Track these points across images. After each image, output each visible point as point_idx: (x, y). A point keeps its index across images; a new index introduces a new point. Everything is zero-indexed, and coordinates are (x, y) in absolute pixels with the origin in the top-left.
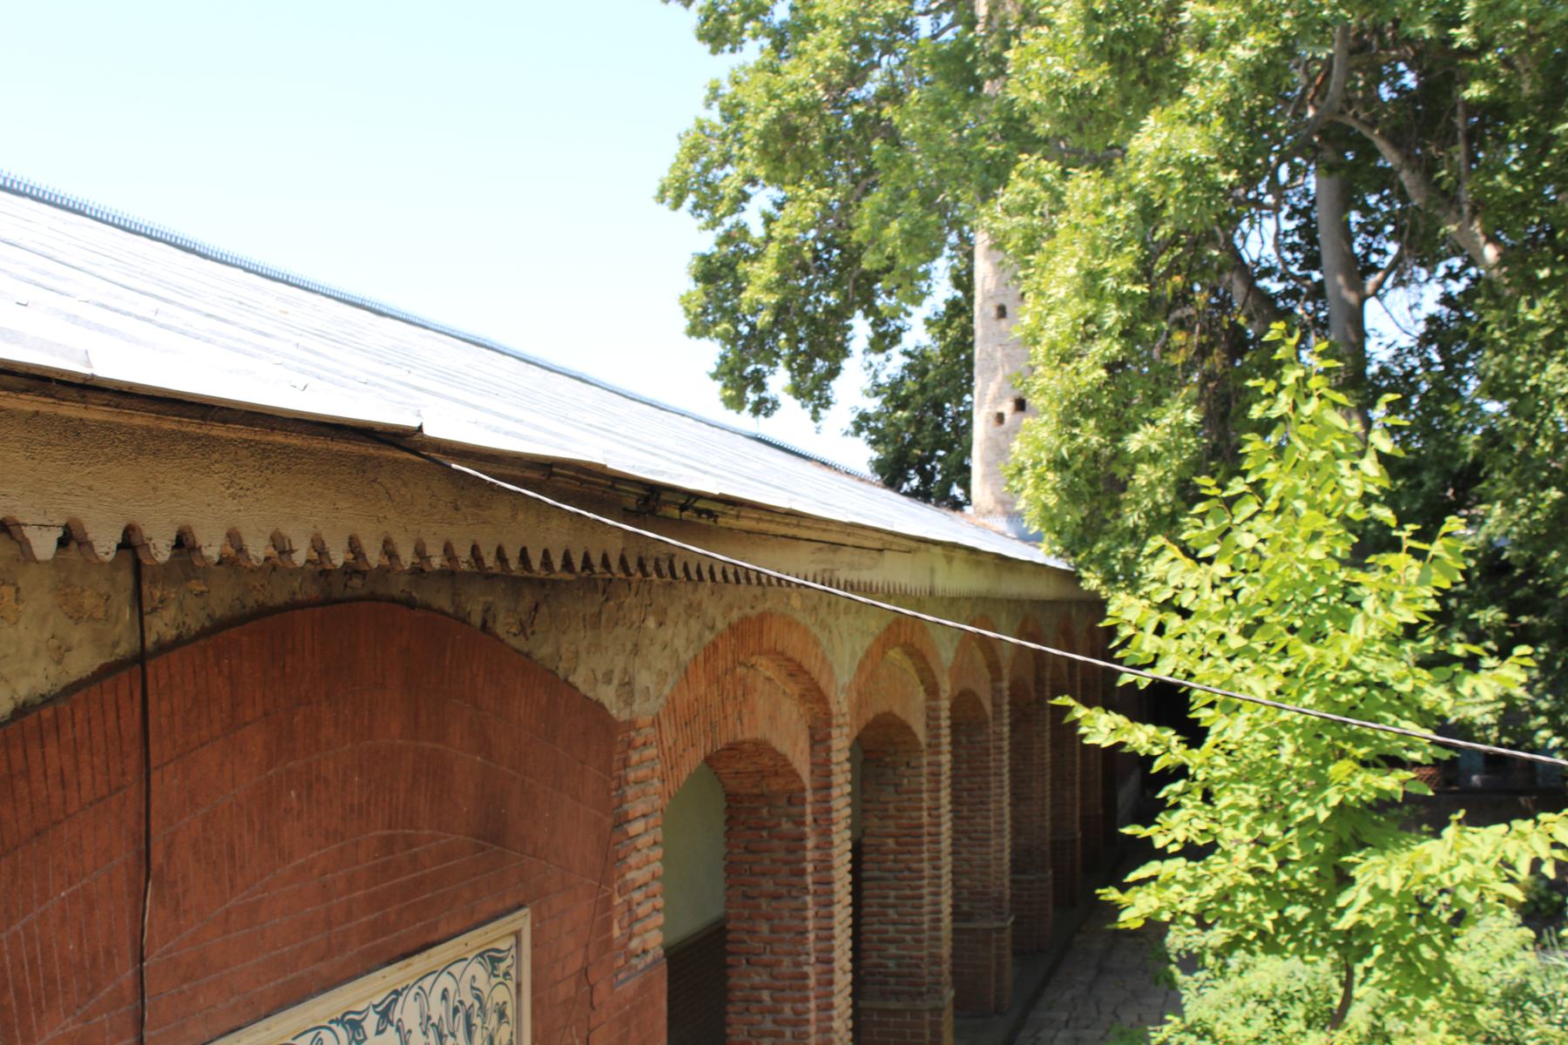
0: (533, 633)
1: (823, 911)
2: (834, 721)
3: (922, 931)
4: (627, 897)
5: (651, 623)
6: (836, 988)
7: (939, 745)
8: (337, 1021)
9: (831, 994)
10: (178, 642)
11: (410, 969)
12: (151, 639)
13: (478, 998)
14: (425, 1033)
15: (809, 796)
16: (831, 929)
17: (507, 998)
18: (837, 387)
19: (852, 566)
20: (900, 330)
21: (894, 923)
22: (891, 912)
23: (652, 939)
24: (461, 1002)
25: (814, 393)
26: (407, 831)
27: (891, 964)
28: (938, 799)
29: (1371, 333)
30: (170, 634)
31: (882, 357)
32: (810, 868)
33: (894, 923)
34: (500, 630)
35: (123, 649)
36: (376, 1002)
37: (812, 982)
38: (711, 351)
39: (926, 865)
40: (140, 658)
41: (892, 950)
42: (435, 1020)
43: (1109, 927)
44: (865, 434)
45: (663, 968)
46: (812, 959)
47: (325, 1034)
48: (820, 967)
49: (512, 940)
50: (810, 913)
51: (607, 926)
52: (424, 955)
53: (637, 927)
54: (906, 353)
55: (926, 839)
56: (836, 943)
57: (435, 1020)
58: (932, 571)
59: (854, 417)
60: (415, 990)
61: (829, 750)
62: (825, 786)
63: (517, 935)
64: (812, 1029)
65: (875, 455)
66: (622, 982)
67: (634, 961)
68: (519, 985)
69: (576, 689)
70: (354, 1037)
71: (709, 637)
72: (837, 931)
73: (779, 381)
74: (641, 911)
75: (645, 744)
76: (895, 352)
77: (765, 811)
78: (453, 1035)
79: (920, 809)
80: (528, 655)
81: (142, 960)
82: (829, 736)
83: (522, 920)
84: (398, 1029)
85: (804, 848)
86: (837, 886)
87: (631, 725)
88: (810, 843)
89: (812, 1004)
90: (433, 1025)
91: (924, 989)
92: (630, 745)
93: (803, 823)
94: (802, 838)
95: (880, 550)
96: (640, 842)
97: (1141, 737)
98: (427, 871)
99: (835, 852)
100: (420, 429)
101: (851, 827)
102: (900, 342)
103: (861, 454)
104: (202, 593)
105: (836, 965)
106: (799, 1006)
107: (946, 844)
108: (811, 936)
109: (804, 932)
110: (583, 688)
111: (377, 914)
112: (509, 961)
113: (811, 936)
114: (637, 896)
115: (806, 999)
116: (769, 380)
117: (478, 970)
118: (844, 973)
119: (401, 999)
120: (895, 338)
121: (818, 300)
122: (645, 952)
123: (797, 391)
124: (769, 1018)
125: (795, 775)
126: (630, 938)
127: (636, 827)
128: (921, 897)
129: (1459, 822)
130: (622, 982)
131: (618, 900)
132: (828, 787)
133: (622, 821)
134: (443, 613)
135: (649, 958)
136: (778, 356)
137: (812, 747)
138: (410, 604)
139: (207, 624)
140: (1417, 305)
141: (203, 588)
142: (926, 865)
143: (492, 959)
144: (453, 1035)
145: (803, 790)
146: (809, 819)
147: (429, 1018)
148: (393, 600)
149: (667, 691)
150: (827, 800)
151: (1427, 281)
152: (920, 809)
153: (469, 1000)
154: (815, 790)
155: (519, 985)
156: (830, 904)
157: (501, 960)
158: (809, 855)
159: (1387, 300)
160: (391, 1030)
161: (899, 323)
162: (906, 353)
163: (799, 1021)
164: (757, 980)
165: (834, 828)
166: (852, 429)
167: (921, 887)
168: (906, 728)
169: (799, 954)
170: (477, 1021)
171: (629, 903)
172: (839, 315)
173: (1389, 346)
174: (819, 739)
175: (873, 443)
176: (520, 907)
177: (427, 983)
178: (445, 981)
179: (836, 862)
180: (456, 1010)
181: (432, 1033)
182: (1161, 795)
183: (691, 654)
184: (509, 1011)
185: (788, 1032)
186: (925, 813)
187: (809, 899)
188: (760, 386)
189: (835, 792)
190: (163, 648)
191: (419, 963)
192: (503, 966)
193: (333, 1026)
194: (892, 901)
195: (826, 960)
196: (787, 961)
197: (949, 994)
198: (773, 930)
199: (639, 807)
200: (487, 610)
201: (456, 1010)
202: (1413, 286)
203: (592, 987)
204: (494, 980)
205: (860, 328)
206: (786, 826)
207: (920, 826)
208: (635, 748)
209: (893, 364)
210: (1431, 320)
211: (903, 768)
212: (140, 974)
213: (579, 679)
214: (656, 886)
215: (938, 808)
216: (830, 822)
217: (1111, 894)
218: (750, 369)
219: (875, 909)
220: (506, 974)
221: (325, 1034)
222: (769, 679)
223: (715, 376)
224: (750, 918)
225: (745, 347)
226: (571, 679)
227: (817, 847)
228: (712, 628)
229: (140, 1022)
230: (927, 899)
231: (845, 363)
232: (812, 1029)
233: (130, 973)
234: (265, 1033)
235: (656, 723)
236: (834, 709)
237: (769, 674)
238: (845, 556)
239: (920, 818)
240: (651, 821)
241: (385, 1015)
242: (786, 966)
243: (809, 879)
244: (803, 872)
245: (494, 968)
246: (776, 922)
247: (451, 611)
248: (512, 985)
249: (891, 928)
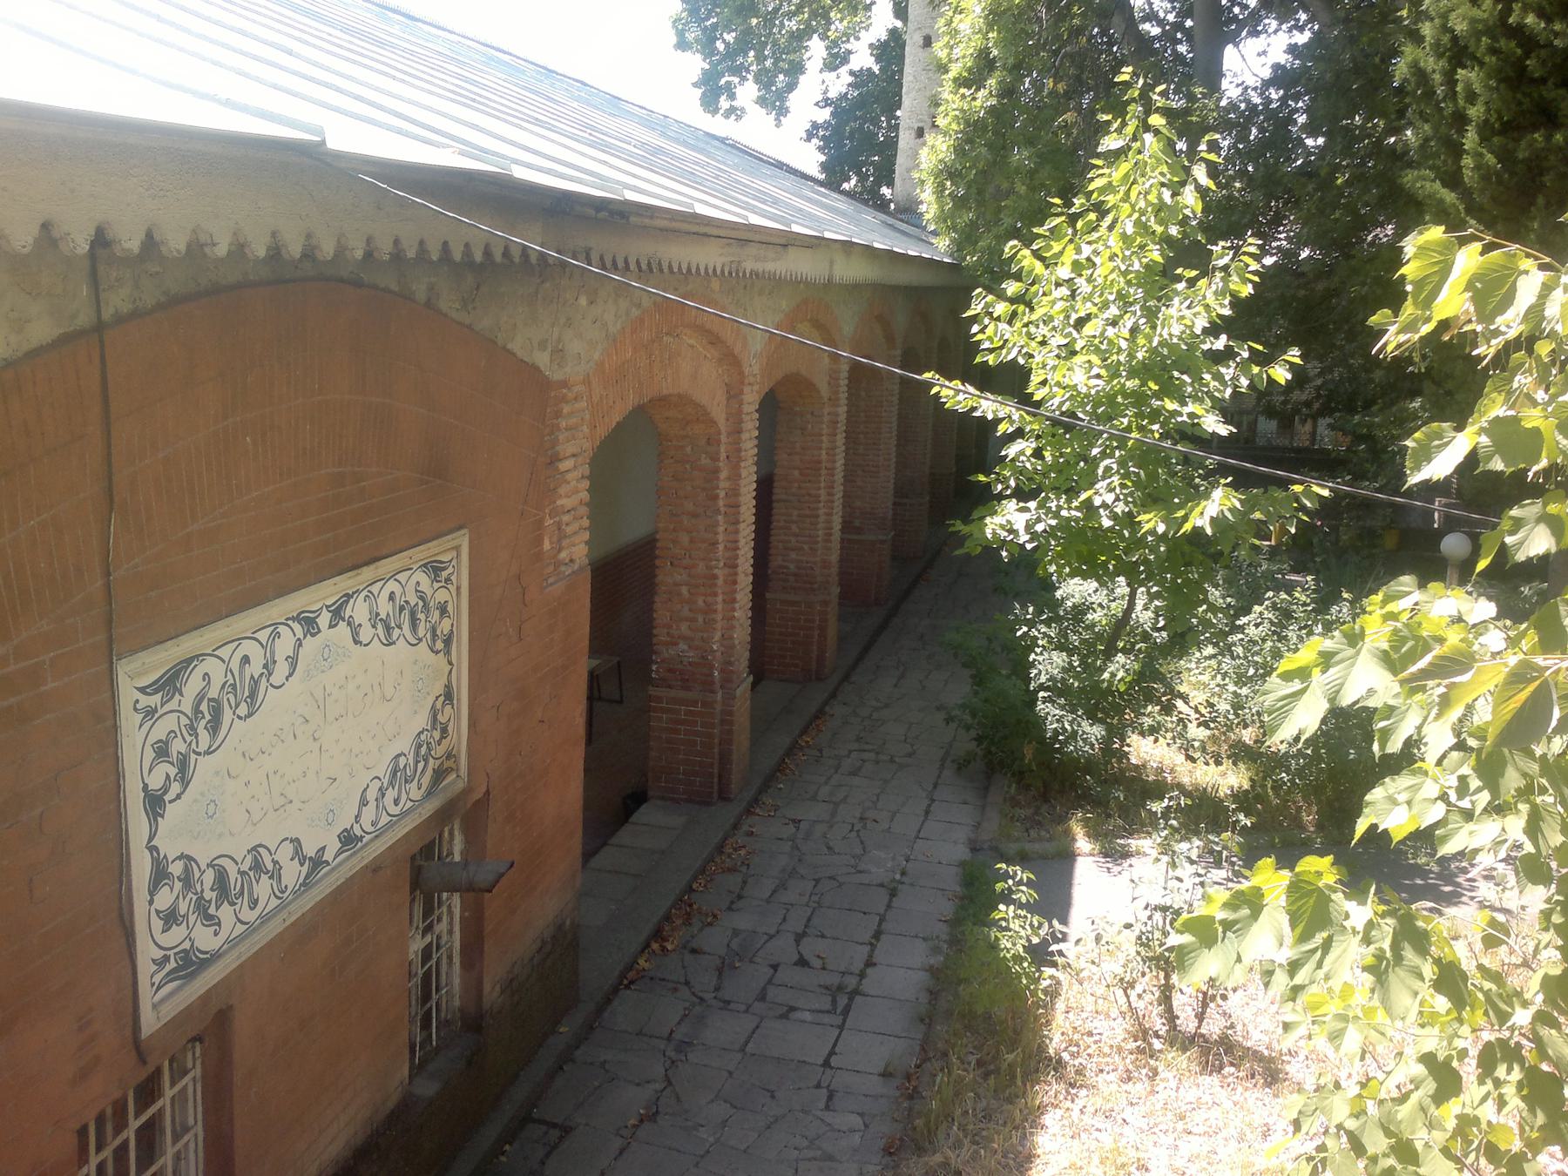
0: (474, 308)
1: (731, 528)
2: (746, 381)
3: (817, 542)
4: (557, 519)
5: (583, 301)
6: (738, 587)
7: (838, 399)
8: (293, 619)
9: (735, 591)
10: (135, 314)
11: (359, 577)
12: (107, 314)
13: (421, 598)
14: (374, 627)
15: (723, 438)
16: (737, 541)
17: (448, 598)
18: (794, 99)
19: (757, 259)
20: (850, 52)
21: (796, 535)
22: (794, 528)
23: (578, 551)
24: (407, 602)
25: (776, 103)
26: (357, 469)
27: (792, 566)
28: (835, 441)
29: (1228, 73)
30: (126, 308)
31: (834, 74)
32: (722, 494)
33: (796, 535)
34: (443, 305)
35: (84, 319)
36: (328, 603)
37: (720, 582)
38: (695, 64)
39: (822, 492)
40: (99, 327)
41: (793, 555)
42: (383, 616)
43: (958, 552)
44: (815, 141)
45: (588, 574)
46: (722, 564)
47: (281, 629)
48: (726, 571)
49: (454, 554)
50: (721, 529)
51: (539, 541)
52: (372, 567)
53: (565, 543)
54: (852, 73)
55: (824, 472)
56: (741, 553)
57: (383, 616)
58: (832, 263)
59: (808, 126)
60: (365, 593)
61: (741, 403)
62: (738, 431)
63: (457, 548)
64: (719, 617)
65: (823, 158)
66: (551, 584)
67: (563, 568)
68: (458, 588)
69: (514, 354)
70: (308, 630)
71: (635, 312)
72: (742, 542)
73: (748, 92)
74: (569, 530)
75: (576, 399)
76: (844, 70)
77: (689, 449)
78: (399, 627)
79: (821, 448)
80: (469, 327)
81: (108, 574)
82: (741, 392)
83: (463, 539)
84: (349, 624)
85: (718, 479)
86: (743, 509)
87: (564, 384)
88: (723, 475)
89: (720, 598)
90: (381, 620)
91: (816, 586)
92: (564, 399)
93: (718, 460)
94: (717, 471)
95: (785, 246)
96: (569, 476)
97: (990, 407)
98: (374, 500)
99: (743, 482)
100: (323, 142)
101: (757, 464)
102: (848, 62)
103: (811, 159)
104: (157, 273)
105: (740, 569)
106: (710, 599)
107: (839, 476)
108: (721, 547)
109: (715, 543)
110: (520, 353)
111: (328, 535)
112: (450, 570)
113: (721, 547)
114: (566, 518)
115: (715, 595)
116: (739, 91)
117: (423, 579)
118: (747, 575)
119: (352, 601)
120: (845, 59)
121: (782, 23)
122: (572, 561)
123: (761, 101)
124: (686, 608)
125: (713, 422)
126: (560, 551)
127: (566, 465)
128: (818, 516)
129: (1225, 485)
130: (551, 584)
131: (548, 522)
132: (739, 432)
133: (555, 459)
134: (391, 292)
135: (576, 567)
136: (748, 71)
137: (728, 400)
138: (358, 284)
139: (163, 299)
140: (1264, 53)
141: (158, 269)
142: (822, 492)
143: (434, 569)
144: (399, 627)
145: (719, 433)
146: (723, 456)
147: (378, 614)
148: (342, 280)
149: (596, 356)
150: (738, 442)
151: (1276, 32)
152: (821, 448)
153: (413, 600)
154: (729, 434)
155: (458, 588)
156: (737, 522)
157: (444, 569)
158: (722, 484)
159: (1241, 46)
160: (342, 625)
161: (848, 46)
162: (852, 73)
163: (709, 610)
164: (678, 578)
165: (742, 464)
166: (805, 136)
167: (818, 509)
168: (810, 386)
169: (711, 560)
170: (421, 616)
171: (559, 525)
172: (799, 37)
173: (1238, 85)
174: (734, 394)
175: (820, 149)
176: (460, 528)
177: (375, 589)
178: (392, 586)
179: (743, 490)
180: (402, 609)
181: (379, 626)
182: (1003, 453)
183: (619, 326)
184: (450, 608)
185: (700, 620)
186: (824, 452)
187: (720, 518)
188: (732, 97)
189: (745, 436)
190: (120, 319)
191: (367, 573)
192: (444, 574)
193: (290, 622)
194: (794, 518)
195: (732, 566)
196: (701, 565)
197: (836, 590)
198: (692, 541)
199: (570, 448)
200: (431, 288)
201: (402, 609)
202: (1263, 36)
203: (524, 589)
204: (436, 585)
205: (816, 49)
206: (705, 461)
207: (820, 462)
208: (567, 402)
209: (839, 83)
210: (1277, 67)
211: (809, 416)
212: (108, 586)
213: (516, 346)
214: (584, 510)
215: (834, 448)
216: (740, 459)
217: (959, 526)
218: (723, 82)
219: (782, 524)
220: (448, 580)
221: (281, 629)
222: (692, 346)
223: (695, 85)
224: (674, 530)
225: (719, 62)
226: (509, 346)
227: (729, 478)
228: (639, 306)
229: (110, 621)
230: (822, 519)
231: (802, 78)
232: (719, 617)
233: (99, 583)
234: (177, 649)
235: (587, 381)
236: (747, 371)
237: (692, 342)
238: (752, 250)
239: (820, 455)
240: (580, 459)
241: (337, 613)
242: (701, 568)
243: (721, 503)
244: (716, 497)
245: (436, 575)
246: (694, 534)
247: (397, 289)
248: (453, 588)
249: (793, 539)
